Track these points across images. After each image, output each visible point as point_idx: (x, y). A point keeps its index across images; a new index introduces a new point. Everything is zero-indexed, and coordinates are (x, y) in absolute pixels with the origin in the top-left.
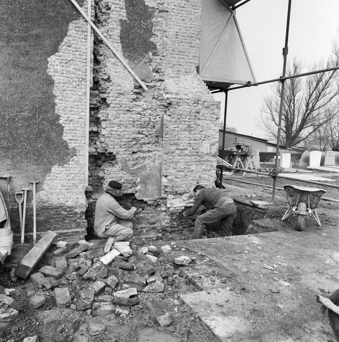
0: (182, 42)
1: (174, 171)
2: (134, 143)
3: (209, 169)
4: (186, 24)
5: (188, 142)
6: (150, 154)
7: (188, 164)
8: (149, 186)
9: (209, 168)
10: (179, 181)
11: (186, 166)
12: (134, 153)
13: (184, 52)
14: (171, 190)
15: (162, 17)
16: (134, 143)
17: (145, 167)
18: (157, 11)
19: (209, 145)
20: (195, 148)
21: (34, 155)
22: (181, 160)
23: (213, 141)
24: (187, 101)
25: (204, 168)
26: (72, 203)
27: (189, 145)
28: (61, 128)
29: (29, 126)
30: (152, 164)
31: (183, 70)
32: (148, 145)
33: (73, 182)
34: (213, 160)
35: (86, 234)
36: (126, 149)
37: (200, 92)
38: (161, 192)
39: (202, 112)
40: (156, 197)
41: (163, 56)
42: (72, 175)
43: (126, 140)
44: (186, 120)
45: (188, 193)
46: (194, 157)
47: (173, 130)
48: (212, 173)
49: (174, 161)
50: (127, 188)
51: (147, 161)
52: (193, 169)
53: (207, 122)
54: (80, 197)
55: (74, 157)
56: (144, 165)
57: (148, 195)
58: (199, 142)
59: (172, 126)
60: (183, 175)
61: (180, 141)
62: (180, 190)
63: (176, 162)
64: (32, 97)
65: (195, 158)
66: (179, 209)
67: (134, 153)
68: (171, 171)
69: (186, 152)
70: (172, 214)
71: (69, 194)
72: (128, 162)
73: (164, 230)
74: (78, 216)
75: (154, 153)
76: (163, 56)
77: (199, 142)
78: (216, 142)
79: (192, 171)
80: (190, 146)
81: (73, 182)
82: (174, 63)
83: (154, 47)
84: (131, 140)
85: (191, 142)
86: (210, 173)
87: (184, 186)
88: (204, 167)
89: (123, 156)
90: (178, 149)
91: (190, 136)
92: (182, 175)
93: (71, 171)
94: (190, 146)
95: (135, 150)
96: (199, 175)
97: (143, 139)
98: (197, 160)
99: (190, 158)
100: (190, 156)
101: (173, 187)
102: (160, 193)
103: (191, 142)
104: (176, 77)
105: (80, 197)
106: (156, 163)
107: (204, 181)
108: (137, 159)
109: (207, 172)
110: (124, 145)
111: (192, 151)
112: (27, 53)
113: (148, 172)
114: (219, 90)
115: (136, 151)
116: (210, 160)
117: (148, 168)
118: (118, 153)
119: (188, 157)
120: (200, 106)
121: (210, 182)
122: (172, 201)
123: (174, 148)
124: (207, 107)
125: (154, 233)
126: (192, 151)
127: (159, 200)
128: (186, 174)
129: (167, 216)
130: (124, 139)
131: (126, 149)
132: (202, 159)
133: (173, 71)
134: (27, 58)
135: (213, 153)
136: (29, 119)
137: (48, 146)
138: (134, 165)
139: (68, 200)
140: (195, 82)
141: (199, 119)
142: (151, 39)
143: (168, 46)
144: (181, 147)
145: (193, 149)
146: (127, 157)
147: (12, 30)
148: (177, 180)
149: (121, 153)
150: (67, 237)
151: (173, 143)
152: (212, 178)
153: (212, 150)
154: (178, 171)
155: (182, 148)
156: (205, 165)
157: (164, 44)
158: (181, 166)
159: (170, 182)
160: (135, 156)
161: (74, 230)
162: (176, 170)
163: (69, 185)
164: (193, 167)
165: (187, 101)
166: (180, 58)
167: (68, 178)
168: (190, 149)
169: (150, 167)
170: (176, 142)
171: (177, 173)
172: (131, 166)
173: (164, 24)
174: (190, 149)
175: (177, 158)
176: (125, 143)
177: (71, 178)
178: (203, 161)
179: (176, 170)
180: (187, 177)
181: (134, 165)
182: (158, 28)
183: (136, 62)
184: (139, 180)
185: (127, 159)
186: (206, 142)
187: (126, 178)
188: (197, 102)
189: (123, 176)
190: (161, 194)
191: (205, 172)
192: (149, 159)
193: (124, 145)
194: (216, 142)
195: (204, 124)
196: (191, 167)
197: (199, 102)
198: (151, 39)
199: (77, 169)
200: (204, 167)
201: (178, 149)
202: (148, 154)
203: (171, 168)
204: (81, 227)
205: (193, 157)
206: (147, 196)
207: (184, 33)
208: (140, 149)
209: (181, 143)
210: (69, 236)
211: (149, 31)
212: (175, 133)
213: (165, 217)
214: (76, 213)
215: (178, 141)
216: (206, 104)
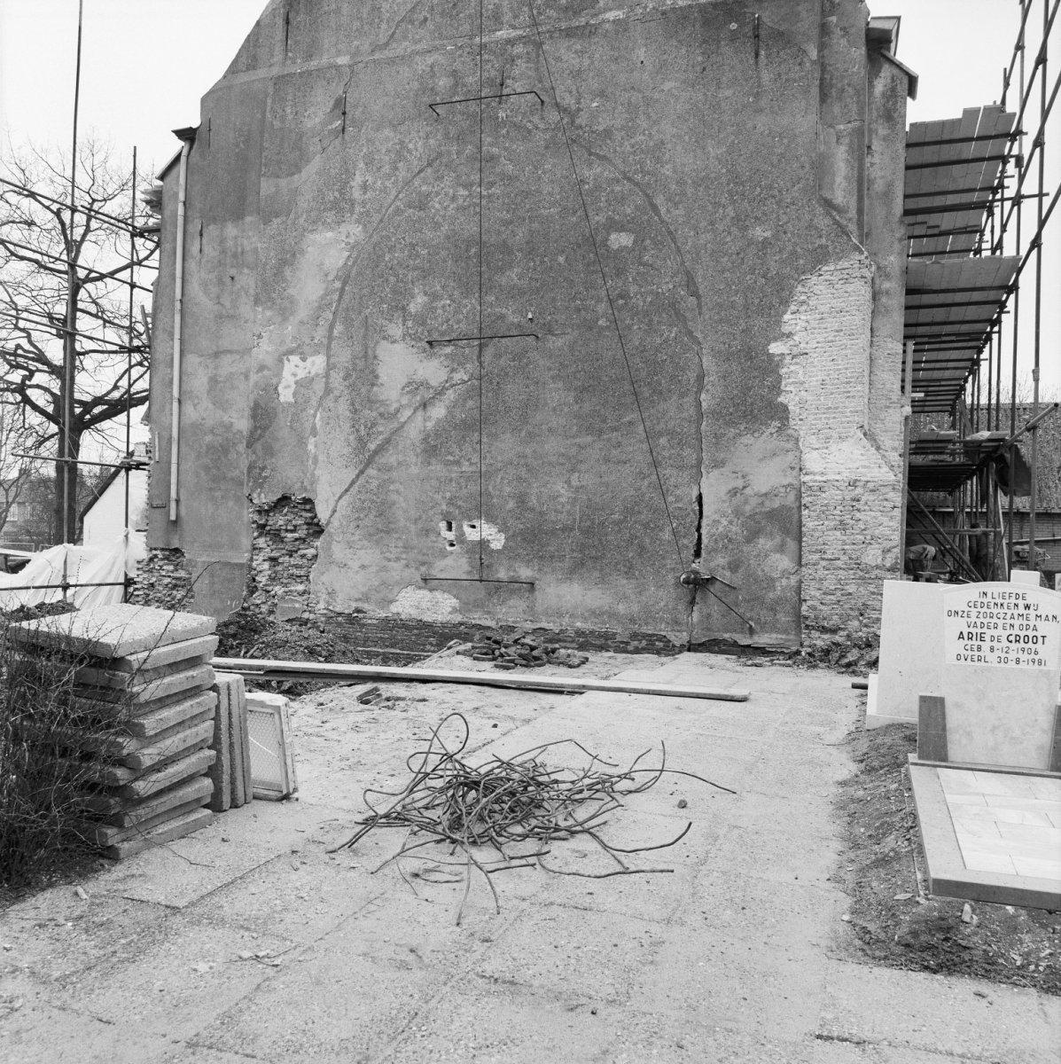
0: (832, 394)
1: (818, 594)
4: (838, 365)
5: (840, 547)
13: (837, 408)
15: (797, 364)
18: (788, 358)
21: (625, 566)
23: (888, 544)
24: (836, 483)
25: (872, 590)
28: (90, 640)
29: (619, 531)
31: (836, 436)
37: (864, 467)
39: (864, 499)
41: (801, 420)
44: (835, 512)
47: (813, 530)
49: (817, 577)
53: (873, 514)
59: (811, 524)
64: (623, 496)
65: (854, 574)
68: (813, 593)
69: (839, 563)
76: (801, 420)
79: (850, 594)
82: (819, 427)
83: (782, 413)
90: (823, 559)
91: (845, 538)
101: (816, 618)
103: (846, 547)
104: (823, 448)
112: (619, 444)
114: (984, 444)
119: (841, 572)
120: (859, 490)
123: (817, 556)
124: (872, 491)
133: (818, 439)
134: (619, 450)
135: (888, 565)
136: (620, 522)
137: (640, 555)
140: (856, 451)
141: (859, 510)
142: (779, 400)
143: (809, 403)
145: (850, 558)
147: (604, 421)
148: (822, 607)
154: (824, 594)
157: (802, 403)
164: (851, 589)
165: (836, 483)
166: (829, 419)
168: (845, 558)
170: (819, 547)
173: (801, 372)
174: (845, 558)
175: (821, 573)
182: (791, 380)
183: (756, 435)
188: (853, 484)
195: (869, 518)
196: (846, 587)
197: (858, 484)
198: (779, 400)
201: (823, 559)
207: (834, 379)
211: (776, 388)
212: (817, 534)
216: (871, 485)
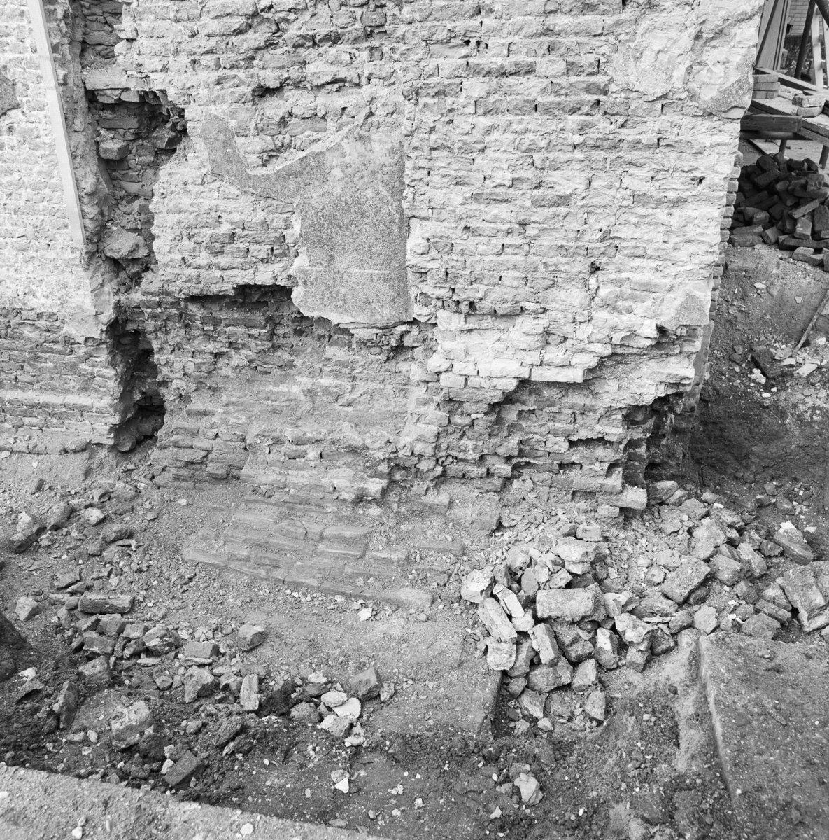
2: (255, 38)
3: (672, 195)
5: (535, 24)
6: (349, 99)
7: (538, 157)
8: (349, 258)
9: (675, 186)
10: (481, 248)
11: (528, 173)
12: (264, 92)
14: (444, 293)
16: (255, 38)
17: (320, 164)
19: (686, 40)
20: (586, 60)
22: (496, 135)
25: (640, 186)
26: (48, 302)
27: (546, 40)
30: (353, 151)
32: (333, 51)
33: (33, 219)
34: (707, 141)
35: (116, 420)
36: (221, 72)
38: (406, 294)
40: (387, 314)
42: (25, 194)
43: (215, 26)
45: (536, 315)
46: (577, 118)
48: (689, 220)
50: (250, 259)
51: (332, 136)
52: (564, 189)
54: (71, 280)
55: (12, 113)
56: (315, 155)
57: (344, 300)
58: (610, 20)
60: (503, 221)
61: (489, 21)
62: (494, 298)
63: (466, 149)
65: (582, 129)
66: (486, 385)
67: (264, 92)
68: (438, 196)
69: (529, 87)
70: (451, 403)
71: (30, 266)
72: (240, 140)
73: (399, 471)
74: (82, 350)
75: (367, 90)
77: (610, 20)
78: (744, 18)
79: (563, 200)
80: (550, 49)
81: (33, 219)
84: (237, 22)
85: (560, 21)
86: (675, 221)
87: (510, 277)
88: (637, 181)
89: (212, 107)
92: (496, 219)
93: (16, 176)
94: (550, 49)
95: (270, 79)
96: (603, 225)
97: (306, 17)
98: (592, 135)
99: (552, 125)
100: (547, 111)
102: (402, 293)
103: (560, 21)
105: (71, 280)
106: (377, 147)
107: (638, 262)
108: (283, 122)
109: (661, 214)
110: (210, 52)
111: (564, 81)
113: (338, 191)
115: (273, 84)
116: (685, 136)
117: (337, 173)
118: (187, 92)
119: (535, 121)
121: (673, 271)
122: (457, 345)
123: (450, 61)
125: (350, 472)
126: (564, 81)
127: (404, 328)
128: (522, 217)
129: (433, 406)
130: (205, 19)
131: (221, 72)
132: (629, 134)
138: (271, 155)
139: (34, 288)
144: (492, 58)
145: (571, 67)
146: (233, 114)
148: (471, 243)
149: (203, 92)
150: (54, 420)
151: (442, 35)
152: (691, 248)
153: (704, 76)
154: (475, 198)
155: (499, 61)
156: (644, 173)
158: (496, 167)
159: (434, 253)
160: (273, 108)
161: (73, 399)
162: (467, 191)
163: (20, 231)
164: (568, 181)
167: (12, 204)
169: (345, 166)
170: (460, 26)
171: (475, 206)
172: (253, 159)
176: (212, 43)
177: (22, 203)
178: (635, 145)
179: (467, 191)
180: (531, 231)
181: (271, 155)
184: (297, 228)
185: (232, 123)
186: (661, 18)
187: (236, 217)
189: (223, 204)
190: (408, 300)
191: (641, 211)
192: (339, 128)
193: (210, 52)
194: (744, 18)
196: (555, 176)
199: (36, 169)
200: (637, 181)
202: (339, 101)
203: (435, 179)
204: (95, 390)
205: (573, 120)
206: (344, 305)
208: (294, 73)
209: (493, 32)
210: (60, 416)
213: (422, 410)
214: (69, 342)
215: (474, 23)
